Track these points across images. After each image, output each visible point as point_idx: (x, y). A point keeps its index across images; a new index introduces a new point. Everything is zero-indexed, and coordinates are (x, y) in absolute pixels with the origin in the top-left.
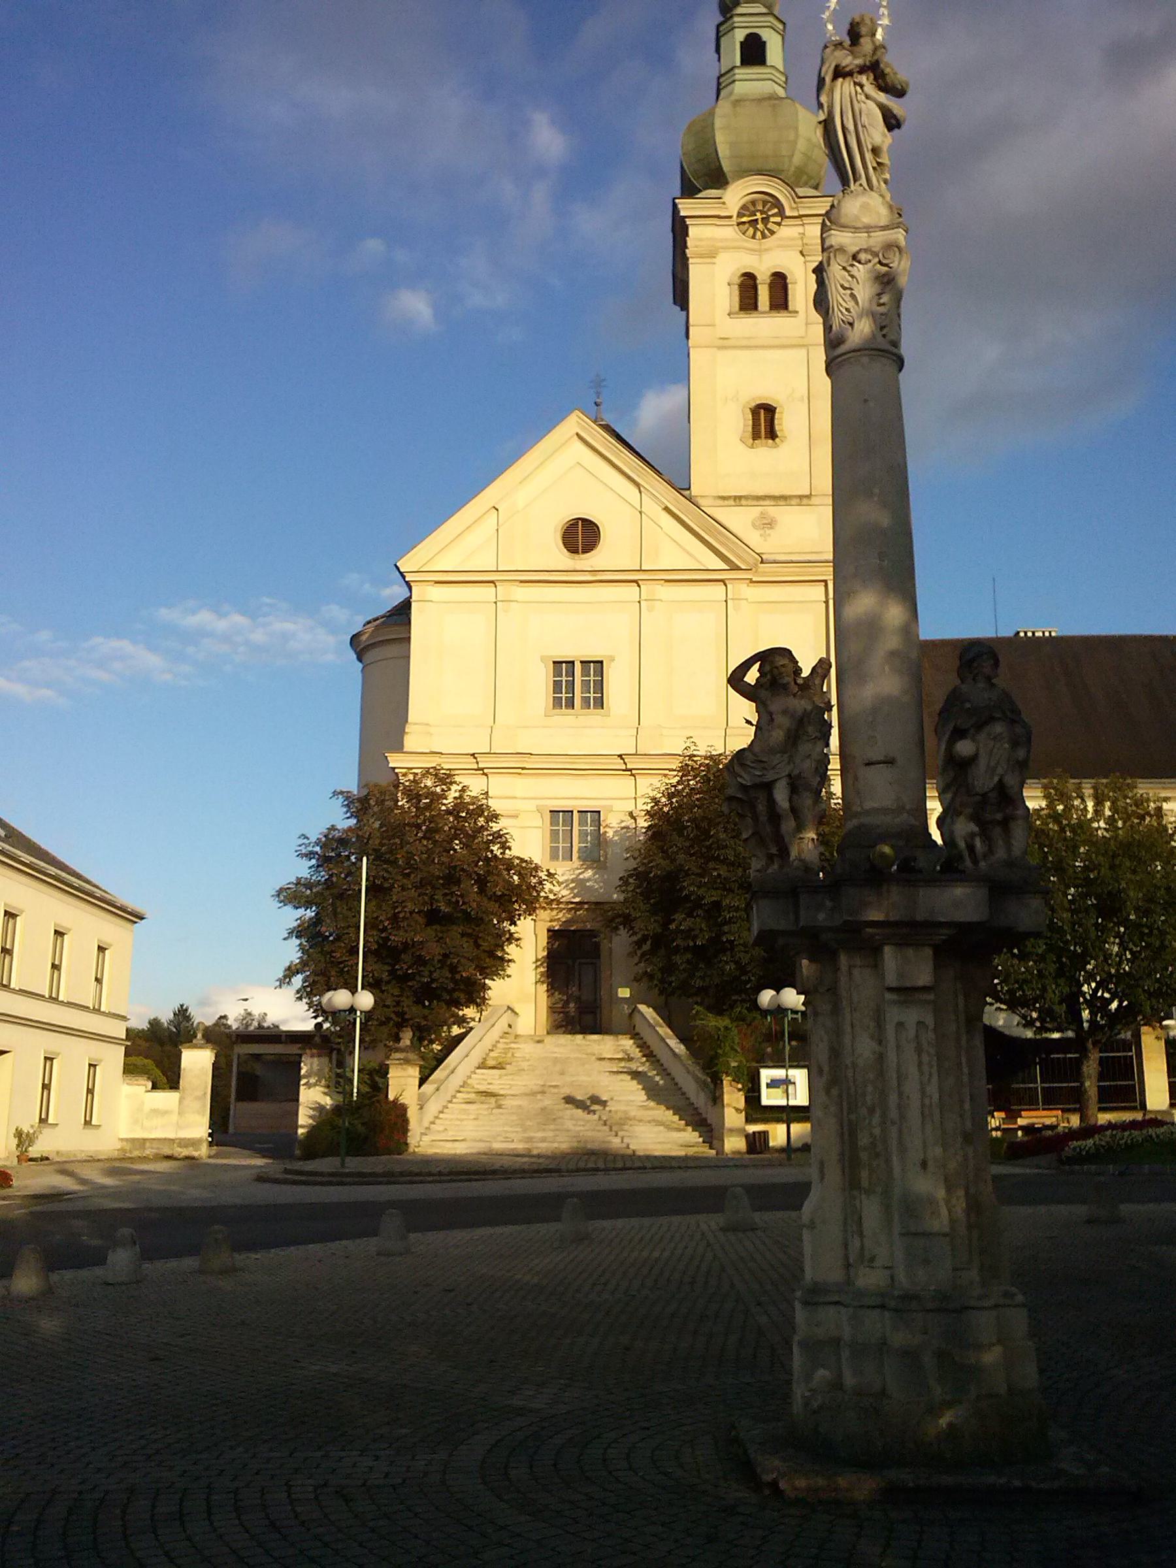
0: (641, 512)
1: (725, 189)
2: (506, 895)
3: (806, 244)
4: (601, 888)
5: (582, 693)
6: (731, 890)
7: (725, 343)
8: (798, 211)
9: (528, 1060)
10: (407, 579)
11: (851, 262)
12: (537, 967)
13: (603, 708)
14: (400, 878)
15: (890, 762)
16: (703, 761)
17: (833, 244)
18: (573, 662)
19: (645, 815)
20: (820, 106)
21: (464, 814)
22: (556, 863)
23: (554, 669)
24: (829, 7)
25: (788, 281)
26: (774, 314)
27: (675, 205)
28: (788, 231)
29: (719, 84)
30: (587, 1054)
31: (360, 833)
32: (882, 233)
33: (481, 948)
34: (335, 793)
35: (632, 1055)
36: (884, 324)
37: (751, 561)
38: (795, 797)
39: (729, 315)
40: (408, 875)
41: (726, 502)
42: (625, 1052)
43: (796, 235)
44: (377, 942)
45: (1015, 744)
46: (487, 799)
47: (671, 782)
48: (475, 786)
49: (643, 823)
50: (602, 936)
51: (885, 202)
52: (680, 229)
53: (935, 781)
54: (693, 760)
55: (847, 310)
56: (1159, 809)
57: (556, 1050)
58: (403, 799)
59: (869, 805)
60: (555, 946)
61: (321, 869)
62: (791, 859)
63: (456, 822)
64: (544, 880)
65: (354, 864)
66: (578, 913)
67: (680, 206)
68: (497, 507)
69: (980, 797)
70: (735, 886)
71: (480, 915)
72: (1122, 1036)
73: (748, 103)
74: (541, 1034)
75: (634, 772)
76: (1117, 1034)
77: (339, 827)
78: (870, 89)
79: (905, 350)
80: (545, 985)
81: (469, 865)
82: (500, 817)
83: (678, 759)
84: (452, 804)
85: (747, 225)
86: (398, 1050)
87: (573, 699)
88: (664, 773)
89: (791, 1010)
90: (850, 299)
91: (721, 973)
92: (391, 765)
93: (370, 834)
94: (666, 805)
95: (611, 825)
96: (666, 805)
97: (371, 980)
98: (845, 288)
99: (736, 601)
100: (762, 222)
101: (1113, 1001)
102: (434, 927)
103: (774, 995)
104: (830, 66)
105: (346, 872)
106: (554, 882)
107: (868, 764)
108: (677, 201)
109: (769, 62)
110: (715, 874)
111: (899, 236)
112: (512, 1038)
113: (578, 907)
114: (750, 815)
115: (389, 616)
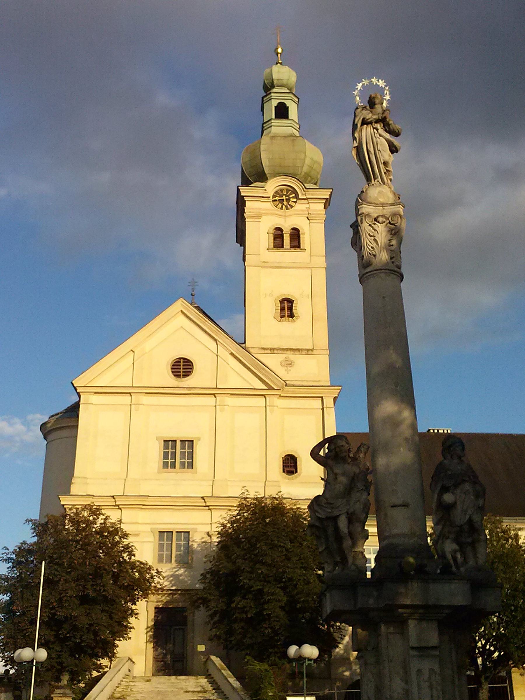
0: (217, 355)
1: (266, 183)
2: (130, 585)
3: (310, 214)
4: (189, 580)
5: (180, 459)
6: (269, 582)
7: (266, 264)
9: (141, 693)
10: (78, 391)
11: (374, 222)
12: (147, 632)
13: (192, 468)
14: (64, 574)
15: (405, 505)
16: (252, 501)
17: (364, 212)
18: (175, 441)
19: (217, 535)
20: (354, 139)
21: (106, 534)
22: (161, 564)
23: (164, 445)
24: (357, 88)
25: (300, 233)
26: (293, 250)
27: (238, 190)
28: (300, 206)
30: (178, 689)
31: (41, 546)
32: (391, 207)
33: (114, 620)
34: (27, 521)
35: (206, 689)
36: (392, 256)
37: (280, 385)
40: (70, 573)
41: (266, 351)
42: (202, 687)
43: (305, 209)
44: (48, 617)
45: (477, 496)
46: (120, 524)
47: (233, 514)
48: (114, 516)
49: (216, 539)
50: (189, 612)
51: (391, 191)
52: (241, 202)
53: (431, 517)
54: (246, 501)
55: (372, 247)
56: (517, 535)
57: (159, 686)
58: (68, 524)
59: (395, 531)
60: (159, 618)
61: (15, 569)
62: (349, 565)
63: (101, 539)
64: (154, 576)
65: (36, 565)
66: (174, 596)
67: (241, 190)
68: (134, 350)
69: (458, 528)
70: (271, 579)
71: (114, 598)
72: (501, 674)
73: (279, 138)
74: (149, 676)
75: (210, 507)
76: (498, 673)
77: (28, 543)
78: (381, 131)
79: (403, 270)
80: (152, 644)
81: (108, 566)
82: (129, 535)
83: (237, 500)
84: (99, 527)
85: (278, 202)
86: (58, 687)
87: (175, 463)
88: (229, 508)
89: (308, 658)
90: (374, 242)
91: (262, 635)
92: (62, 503)
93: (47, 546)
94: (230, 528)
95: (196, 541)
96: (230, 528)
97: (43, 641)
98: (371, 236)
99: (271, 407)
100: (286, 201)
101: (495, 652)
102: (85, 606)
103: (297, 649)
104: (360, 118)
105: (30, 571)
106: (161, 577)
107: (393, 507)
108: (239, 187)
109: (290, 118)
110: (260, 572)
111: (400, 209)
112: (130, 678)
113: (174, 592)
114: (323, 537)
115: (66, 412)
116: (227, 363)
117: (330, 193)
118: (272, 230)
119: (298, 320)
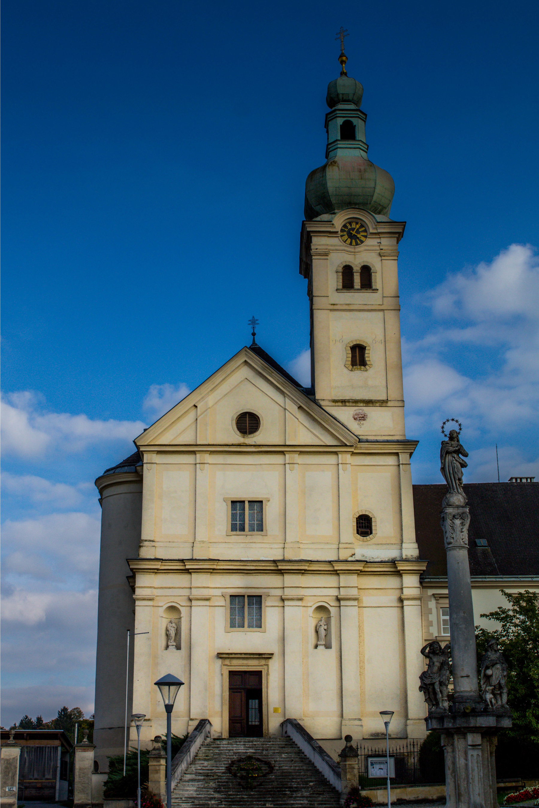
8: (377, 230)
15: (468, 676)
25: (372, 271)
28: (371, 242)
29: (327, 149)
38: (441, 687)
39: (337, 290)
41: (337, 404)
59: (462, 689)
68: (196, 405)
107: (461, 677)
116: (296, 418)
117: (403, 227)
118: (341, 268)
119: (371, 369)
